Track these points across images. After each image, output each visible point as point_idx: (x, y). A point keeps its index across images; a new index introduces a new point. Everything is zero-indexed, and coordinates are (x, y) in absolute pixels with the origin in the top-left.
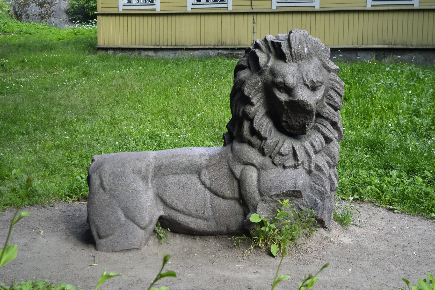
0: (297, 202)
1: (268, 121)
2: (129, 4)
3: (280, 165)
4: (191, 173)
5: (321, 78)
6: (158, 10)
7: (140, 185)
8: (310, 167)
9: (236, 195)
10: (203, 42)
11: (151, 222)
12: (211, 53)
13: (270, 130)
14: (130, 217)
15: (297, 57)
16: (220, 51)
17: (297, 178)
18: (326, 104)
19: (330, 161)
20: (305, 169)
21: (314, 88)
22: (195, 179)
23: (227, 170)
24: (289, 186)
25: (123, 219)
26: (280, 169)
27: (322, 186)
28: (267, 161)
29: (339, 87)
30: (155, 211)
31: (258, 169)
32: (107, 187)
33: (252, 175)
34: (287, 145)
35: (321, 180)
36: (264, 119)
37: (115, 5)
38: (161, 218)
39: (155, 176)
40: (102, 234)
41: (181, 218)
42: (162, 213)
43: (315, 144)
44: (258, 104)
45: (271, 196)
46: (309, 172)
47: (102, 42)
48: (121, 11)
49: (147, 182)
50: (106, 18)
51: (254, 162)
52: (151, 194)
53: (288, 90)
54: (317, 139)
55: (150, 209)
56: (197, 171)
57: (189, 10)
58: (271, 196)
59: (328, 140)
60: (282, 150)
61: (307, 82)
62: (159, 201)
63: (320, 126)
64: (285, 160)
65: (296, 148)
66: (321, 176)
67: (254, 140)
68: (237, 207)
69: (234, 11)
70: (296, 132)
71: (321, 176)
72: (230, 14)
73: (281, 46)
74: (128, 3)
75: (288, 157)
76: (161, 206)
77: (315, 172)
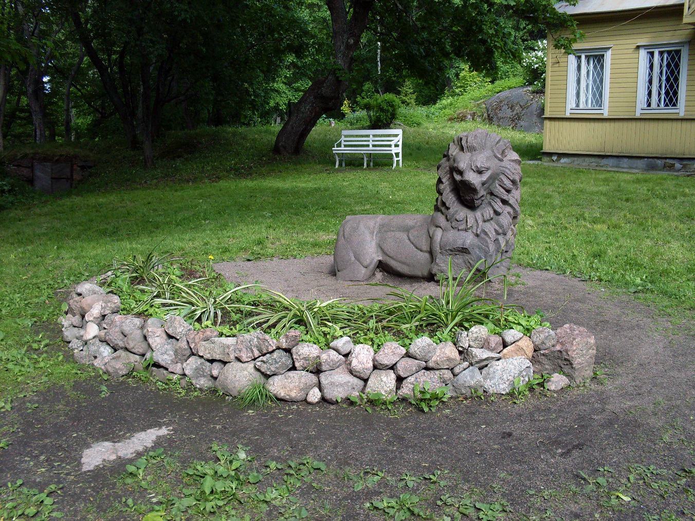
0: (467, 257)
1: (453, 196)
2: (649, 108)
3: (456, 228)
4: (403, 231)
5: (486, 165)
6: (606, 115)
7: (368, 237)
8: (477, 231)
9: (429, 250)
10: (678, 151)
11: (371, 263)
12: (659, 162)
13: (454, 203)
14: (358, 259)
15: (472, 149)
16: (667, 161)
17: (468, 239)
18: (497, 185)
19: (497, 228)
20: (473, 232)
21: (480, 172)
22: (404, 236)
23: (426, 231)
24: (459, 244)
25: (353, 259)
26: (456, 230)
27: (488, 247)
28: (448, 225)
29: (509, 172)
30: (374, 255)
31: (443, 231)
32: (346, 236)
33: (439, 234)
34: (463, 213)
35: (487, 242)
36: (450, 194)
37: (563, 109)
38: (380, 261)
39: (379, 232)
40: (339, 268)
41: (393, 264)
42: (380, 258)
43: (485, 215)
44: (447, 183)
45: (446, 250)
46: (477, 235)
47: (547, 148)
48: (568, 115)
49: (373, 235)
50: (553, 123)
51: (441, 225)
52: (374, 243)
53: (461, 173)
54: (487, 211)
55: (372, 255)
56: (407, 230)
57: (638, 115)
58: (446, 250)
59: (497, 213)
60: (457, 217)
61: (473, 167)
62: (379, 250)
63: (493, 203)
64: (460, 225)
65: (469, 216)
66: (487, 239)
67: (443, 209)
68: (427, 255)
69: (686, 117)
70: (471, 205)
71: (487, 239)
72: (682, 120)
73: (216, 126)
74: (648, 106)
75: (462, 222)
76: (380, 253)
77: (483, 235)
